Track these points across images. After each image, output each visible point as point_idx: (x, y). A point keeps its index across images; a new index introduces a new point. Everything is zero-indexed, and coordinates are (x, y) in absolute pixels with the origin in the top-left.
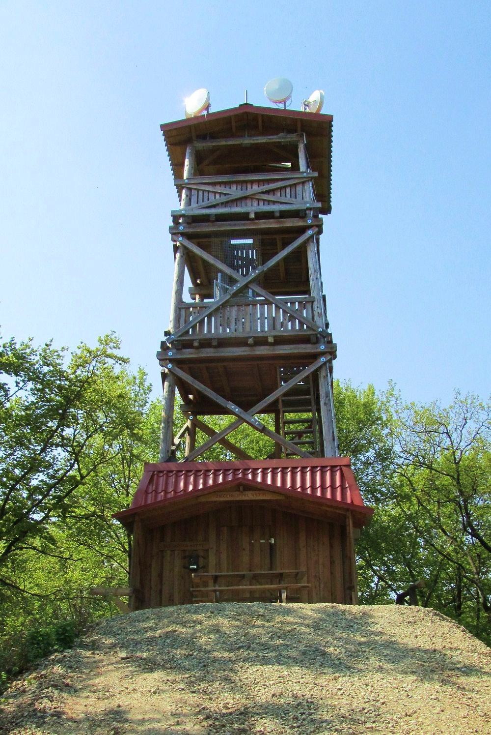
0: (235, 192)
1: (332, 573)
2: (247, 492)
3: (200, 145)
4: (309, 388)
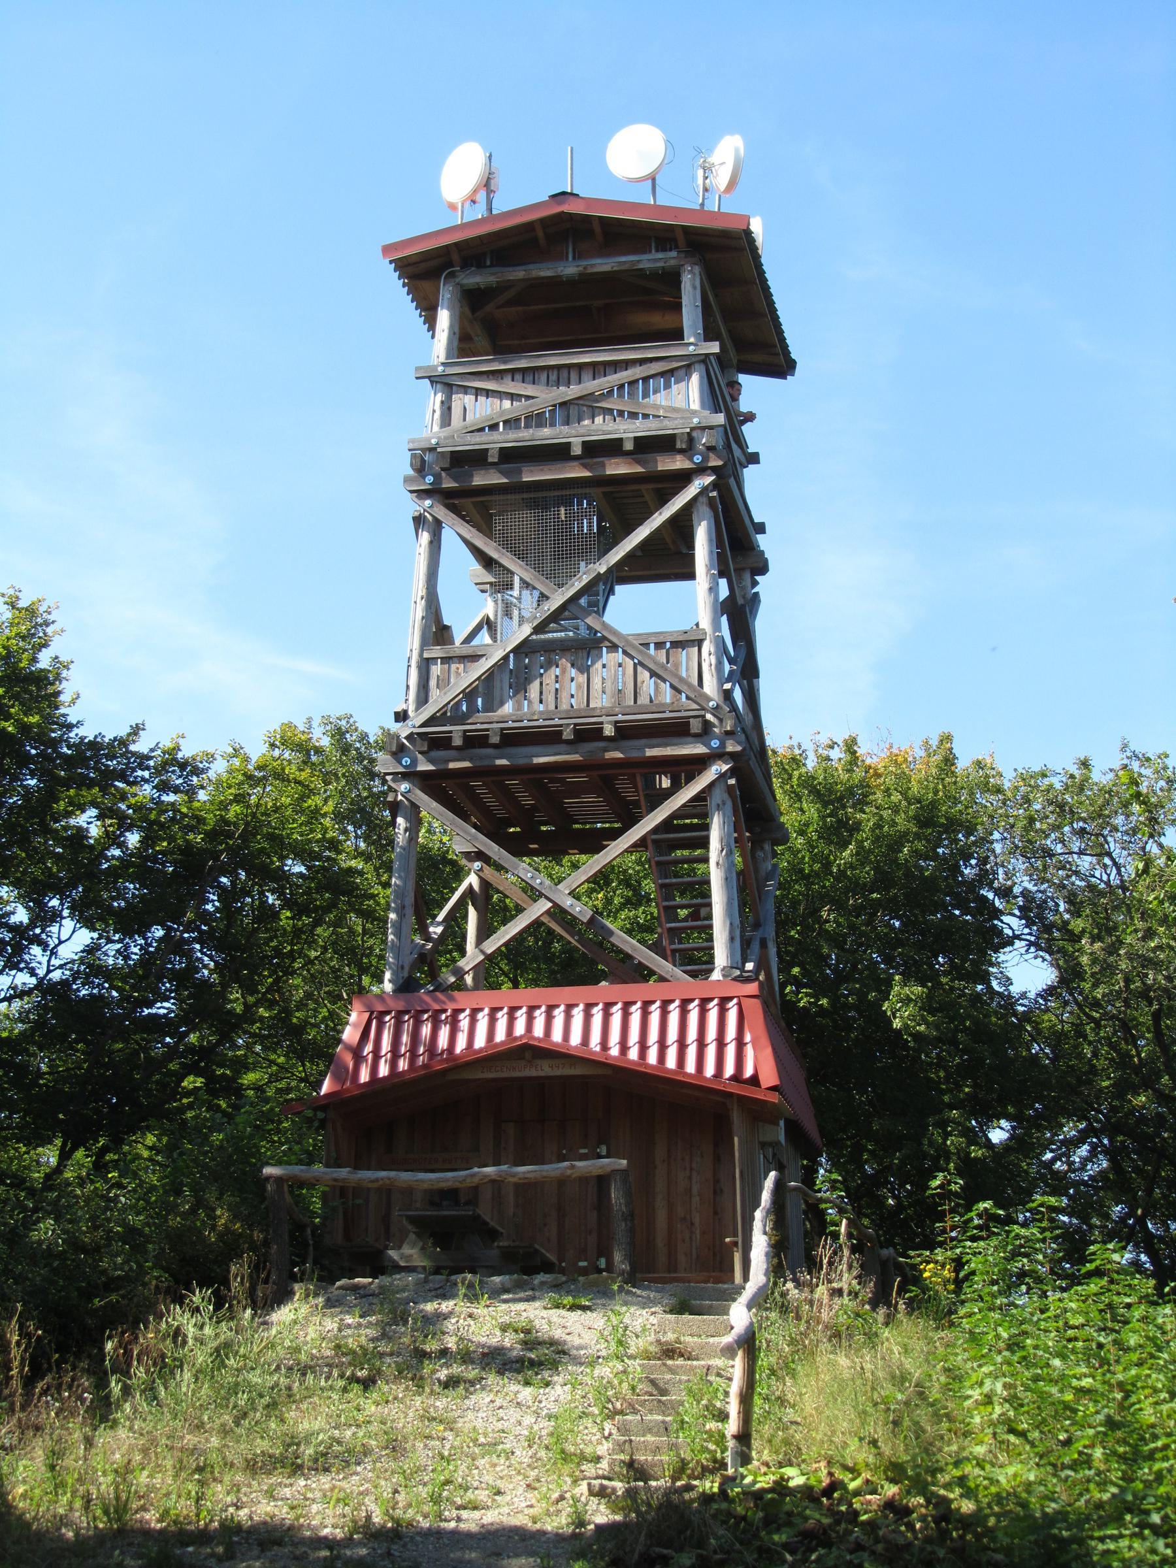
0: (545, 396)
1: (716, 1213)
2: (539, 1062)
3: (475, 279)
4: (520, 910)
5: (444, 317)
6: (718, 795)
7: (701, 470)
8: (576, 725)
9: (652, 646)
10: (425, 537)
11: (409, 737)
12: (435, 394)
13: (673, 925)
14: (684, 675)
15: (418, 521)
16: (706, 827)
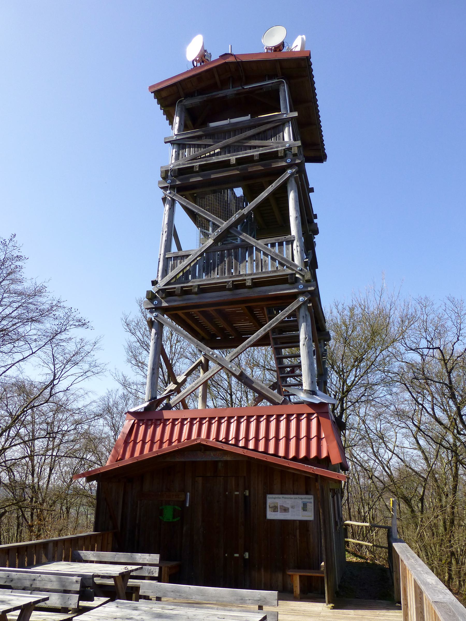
3: (189, 102)
5: (177, 119)
6: (303, 312)
7: (290, 166)
8: (233, 281)
9: (269, 245)
10: (167, 207)
11: (157, 292)
12: (173, 149)
13: (283, 375)
14: (285, 256)
15: (164, 200)
16: (298, 330)
